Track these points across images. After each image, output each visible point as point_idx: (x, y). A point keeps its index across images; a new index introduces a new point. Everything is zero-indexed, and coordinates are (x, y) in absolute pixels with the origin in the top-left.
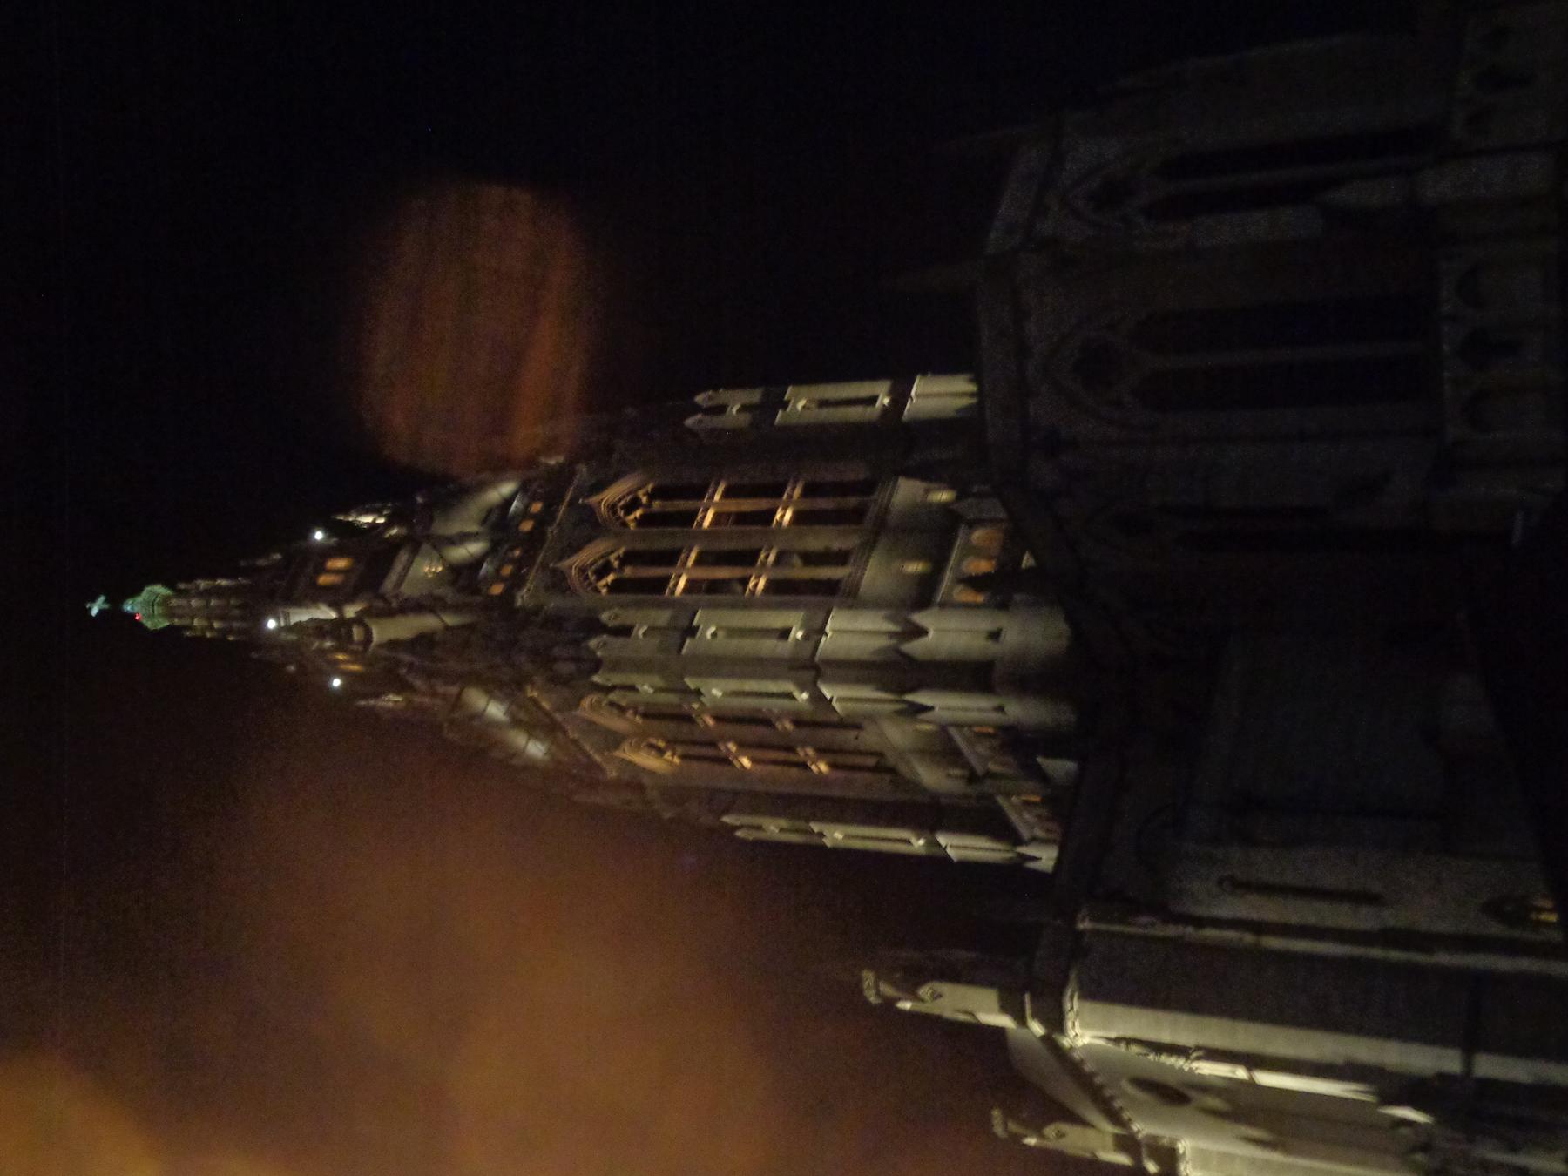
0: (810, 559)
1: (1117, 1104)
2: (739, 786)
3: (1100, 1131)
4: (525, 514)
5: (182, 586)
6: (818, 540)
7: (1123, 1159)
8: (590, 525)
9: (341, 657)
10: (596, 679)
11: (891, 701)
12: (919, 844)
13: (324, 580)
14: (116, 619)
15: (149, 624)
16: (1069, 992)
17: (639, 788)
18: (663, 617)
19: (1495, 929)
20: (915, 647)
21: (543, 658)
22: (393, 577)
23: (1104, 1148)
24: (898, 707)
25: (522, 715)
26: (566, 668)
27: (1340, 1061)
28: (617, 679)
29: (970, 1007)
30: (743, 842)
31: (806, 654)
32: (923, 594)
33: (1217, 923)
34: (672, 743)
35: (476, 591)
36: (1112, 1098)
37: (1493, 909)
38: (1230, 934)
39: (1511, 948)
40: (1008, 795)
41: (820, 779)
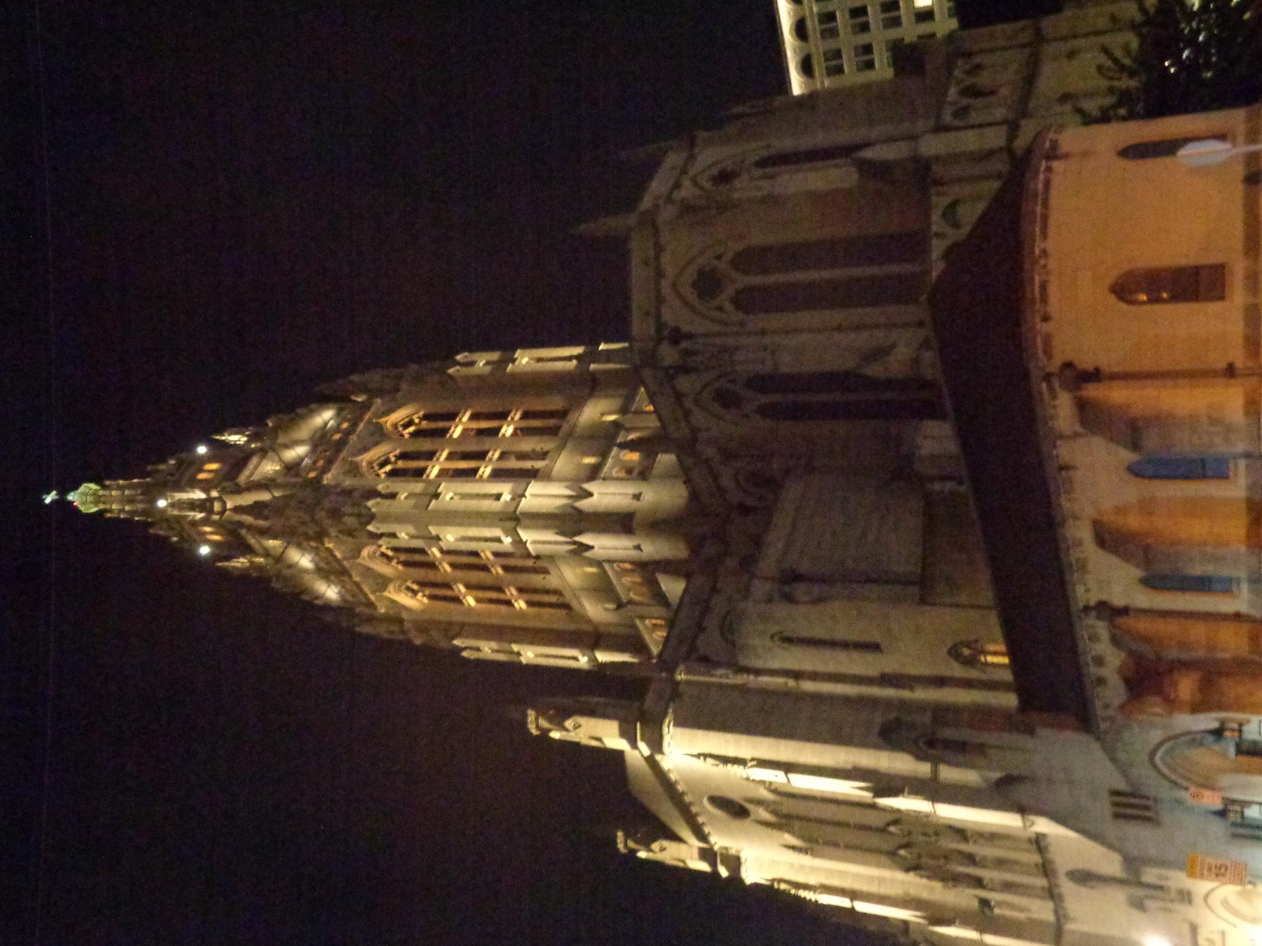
0: (522, 456)
1: (700, 820)
2: (467, 620)
3: (690, 846)
4: (337, 429)
5: (108, 483)
6: (527, 445)
7: (704, 867)
8: (379, 435)
9: (208, 529)
10: (370, 528)
11: (567, 543)
12: (583, 661)
13: (201, 476)
14: (63, 505)
15: (82, 509)
16: (667, 721)
17: (400, 621)
18: (418, 487)
19: (957, 670)
20: (584, 504)
21: (335, 514)
22: (246, 473)
23: (691, 858)
24: (572, 547)
25: (322, 565)
26: (350, 521)
27: (849, 767)
28: (384, 528)
29: (598, 735)
30: (466, 660)
31: (511, 509)
32: (594, 473)
33: (773, 673)
34: (423, 584)
35: (298, 475)
36: (696, 815)
37: (954, 653)
38: (780, 680)
39: (968, 684)
40: (642, 618)
41: (521, 614)
